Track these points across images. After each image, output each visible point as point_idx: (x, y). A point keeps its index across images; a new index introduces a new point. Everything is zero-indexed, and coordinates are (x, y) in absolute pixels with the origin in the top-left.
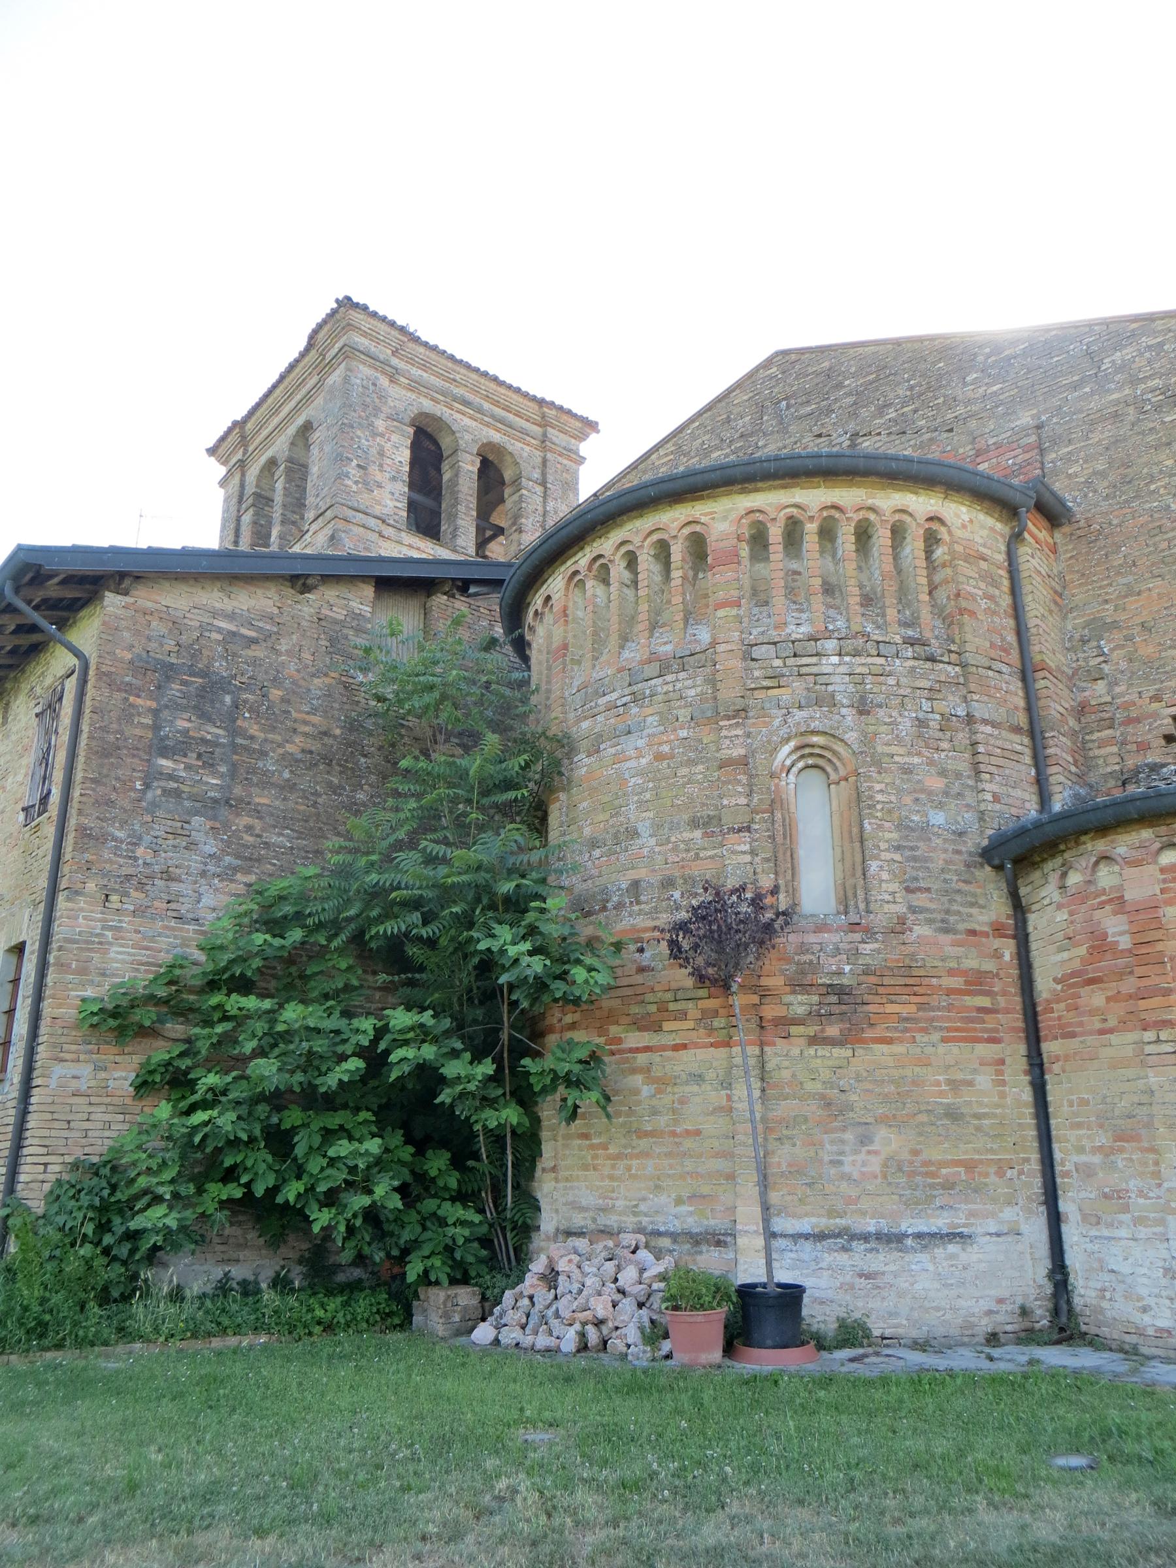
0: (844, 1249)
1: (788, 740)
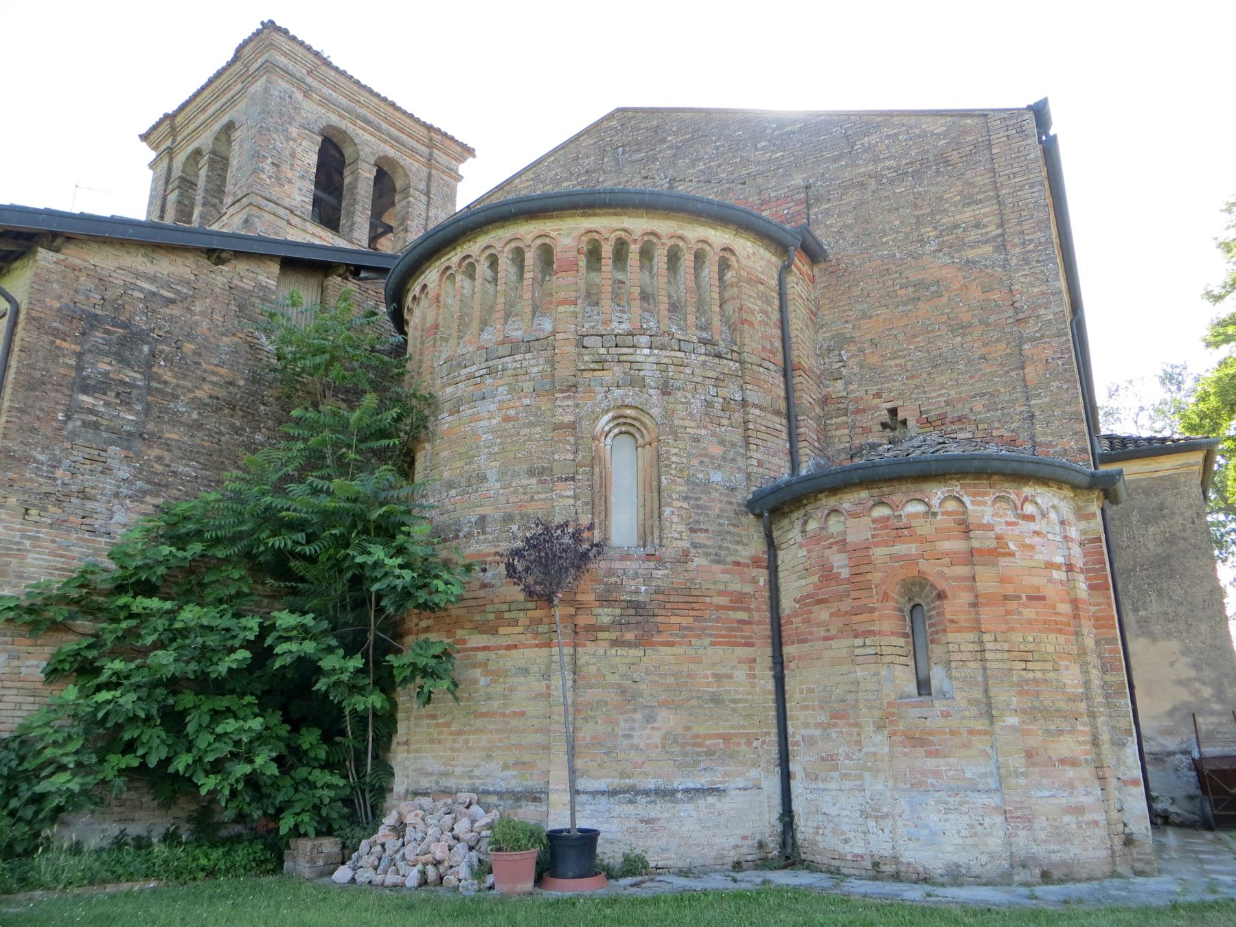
0: (631, 802)
1: (607, 411)
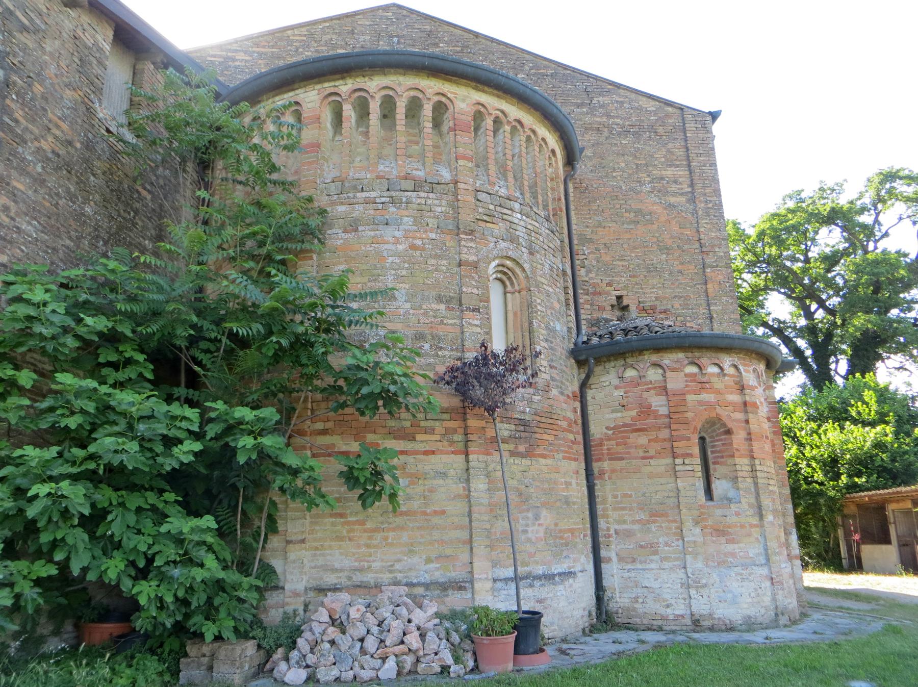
0: (531, 586)
